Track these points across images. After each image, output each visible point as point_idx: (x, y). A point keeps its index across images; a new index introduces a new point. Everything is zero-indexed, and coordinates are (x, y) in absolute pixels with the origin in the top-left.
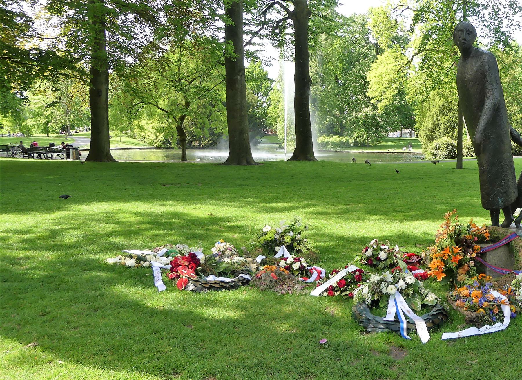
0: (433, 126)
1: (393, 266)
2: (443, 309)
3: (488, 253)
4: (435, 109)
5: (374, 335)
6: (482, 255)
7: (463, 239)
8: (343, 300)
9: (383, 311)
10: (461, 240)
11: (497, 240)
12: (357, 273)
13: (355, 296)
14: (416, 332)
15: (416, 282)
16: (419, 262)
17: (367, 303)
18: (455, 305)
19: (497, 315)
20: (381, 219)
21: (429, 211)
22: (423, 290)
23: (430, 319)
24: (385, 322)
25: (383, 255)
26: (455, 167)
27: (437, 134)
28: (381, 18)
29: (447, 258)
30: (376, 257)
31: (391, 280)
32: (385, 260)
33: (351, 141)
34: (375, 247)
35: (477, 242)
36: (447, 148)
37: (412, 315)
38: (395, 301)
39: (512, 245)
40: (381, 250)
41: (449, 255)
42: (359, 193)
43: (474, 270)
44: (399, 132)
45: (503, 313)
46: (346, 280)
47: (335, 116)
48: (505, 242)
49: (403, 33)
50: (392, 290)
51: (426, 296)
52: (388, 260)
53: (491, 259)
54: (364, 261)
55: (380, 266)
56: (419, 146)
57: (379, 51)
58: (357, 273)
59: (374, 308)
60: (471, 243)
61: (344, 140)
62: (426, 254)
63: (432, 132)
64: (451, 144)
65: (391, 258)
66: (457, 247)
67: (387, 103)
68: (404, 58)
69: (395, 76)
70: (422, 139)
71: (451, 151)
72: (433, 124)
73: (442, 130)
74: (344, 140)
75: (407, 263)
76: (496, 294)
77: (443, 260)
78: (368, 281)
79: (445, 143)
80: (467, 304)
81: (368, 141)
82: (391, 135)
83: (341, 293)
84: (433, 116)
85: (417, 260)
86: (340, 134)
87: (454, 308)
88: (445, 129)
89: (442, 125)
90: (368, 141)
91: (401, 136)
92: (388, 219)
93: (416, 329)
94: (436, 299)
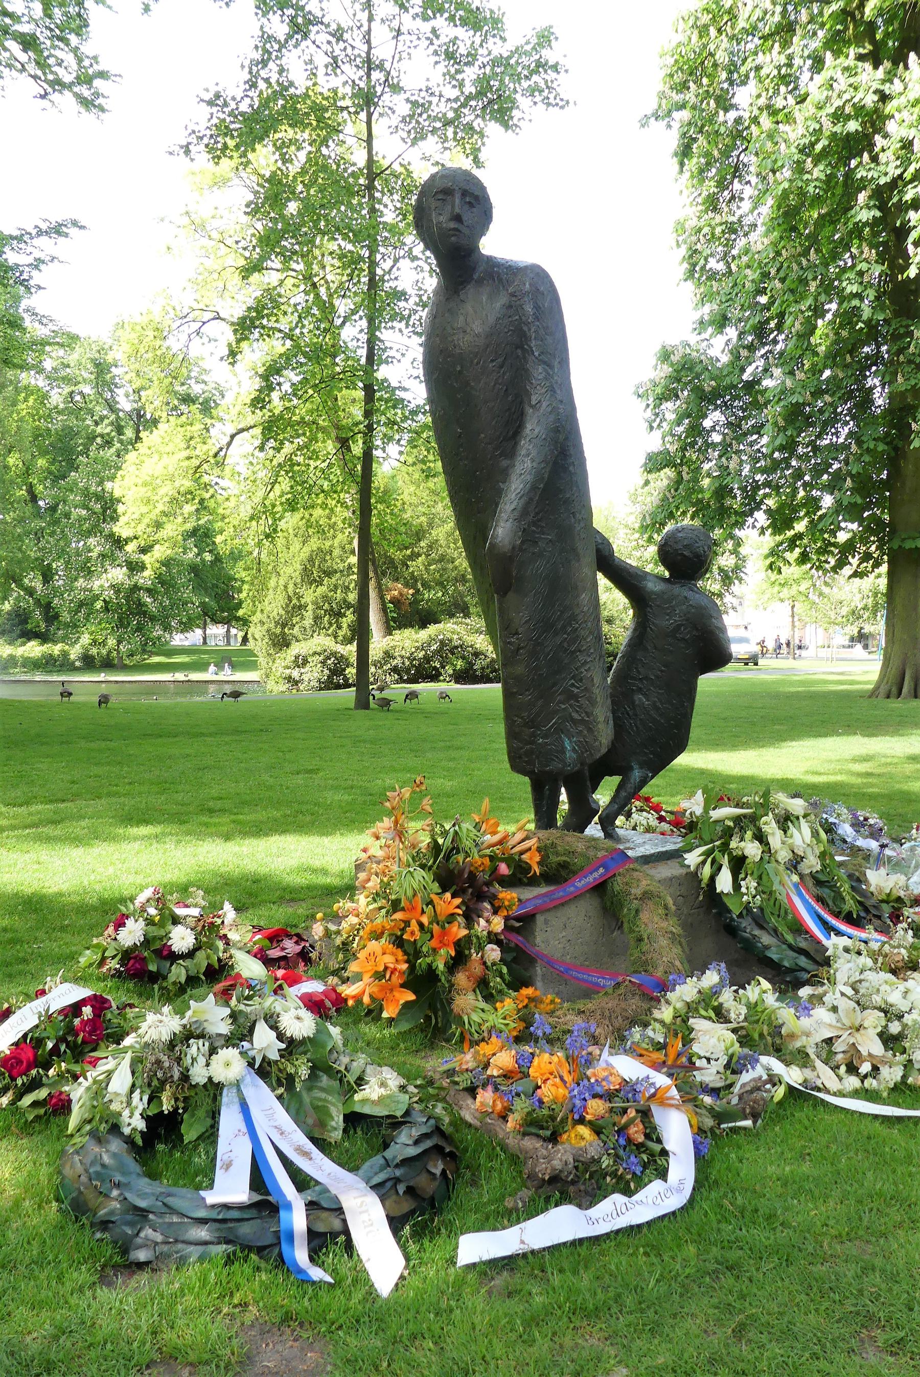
0: (287, 612)
1: (218, 974)
2: (438, 1130)
3: (540, 919)
4: (289, 570)
5: (169, 1281)
6: (522, 923)
7: (461, 872)
8: (27, 1129)
9: (199, 1160)
10: (458, 877)
11: (563, 873)
12: (87, 1011)
13: (75, 1108)
14: (349, 1246)
15: (318, 1031)
16: (304, 955)
17: (127, 1131)
18: (469, 1110)
19: (640, 1146)
20: (164, 834)
21: (304, 808)
22: (345, 1060)
23: (397, 1180)
24: (213, 1215)
25: (181, 939)
26: (352, 705)
27: (296, 631)
28: (147, 339)
29: (417, 933)
30: (157, 945)
31: (224, 1028)
32: (191, 954)
33: (75, 653)
34: (152, 911)
35: (509, 882)
36: (323, 663)
37: (320, 1167)
38: (245, 1108)
39: (617, 888)
40: (176, 920)
41: (421, 925)
42: (96, 770)
43: (501, 976)
44: (199, 632)
45: (659, 1141)
46: (39, 1042)
47: (30, 592)
48: (591, 879)
49: (203, 386)
50: (228, 1066)
51: (361, 1081)
52: (201, 955)
53: (554, 938)
54: (114, 964)
55: (172, 978)
56: (252, 666)
57: (142, 421)
58: (87, 1011)
59: (161, 1147)
60: (488, 884)
61: (56, 652)
62: (327, 929)
63: (284, 626)
64: (334, 654)
65: (212, 946)
66: (448, 895)
67: (169, 552)
68: (209, 441)
69: (187, 484)
70: (259, 644)
71: (337, 670)
72: (287, 606)
73: (308, 622)
74: (56, 652)
75: (268, 962)
76: (627, 1067)
77: (399, 942)
78: (128, 1041)
79: (319, 649)
80: (521, 1106)
81: (118, 653)
82: (178, 640)
83: (19, 1096)
84: (286, 587)
85: (298, 949)
86: (44, 638)
87: (468, 1118)
88: (317, 619)
89: (310, 607)
90: (118, 653)
91: (205, 643)
92: (188, 833)
93: (347, 1232)
94: (403, 1088)
